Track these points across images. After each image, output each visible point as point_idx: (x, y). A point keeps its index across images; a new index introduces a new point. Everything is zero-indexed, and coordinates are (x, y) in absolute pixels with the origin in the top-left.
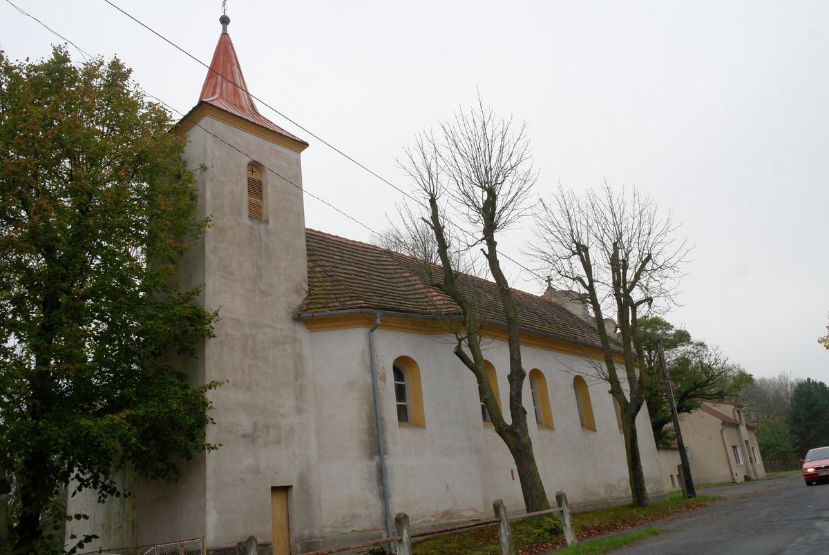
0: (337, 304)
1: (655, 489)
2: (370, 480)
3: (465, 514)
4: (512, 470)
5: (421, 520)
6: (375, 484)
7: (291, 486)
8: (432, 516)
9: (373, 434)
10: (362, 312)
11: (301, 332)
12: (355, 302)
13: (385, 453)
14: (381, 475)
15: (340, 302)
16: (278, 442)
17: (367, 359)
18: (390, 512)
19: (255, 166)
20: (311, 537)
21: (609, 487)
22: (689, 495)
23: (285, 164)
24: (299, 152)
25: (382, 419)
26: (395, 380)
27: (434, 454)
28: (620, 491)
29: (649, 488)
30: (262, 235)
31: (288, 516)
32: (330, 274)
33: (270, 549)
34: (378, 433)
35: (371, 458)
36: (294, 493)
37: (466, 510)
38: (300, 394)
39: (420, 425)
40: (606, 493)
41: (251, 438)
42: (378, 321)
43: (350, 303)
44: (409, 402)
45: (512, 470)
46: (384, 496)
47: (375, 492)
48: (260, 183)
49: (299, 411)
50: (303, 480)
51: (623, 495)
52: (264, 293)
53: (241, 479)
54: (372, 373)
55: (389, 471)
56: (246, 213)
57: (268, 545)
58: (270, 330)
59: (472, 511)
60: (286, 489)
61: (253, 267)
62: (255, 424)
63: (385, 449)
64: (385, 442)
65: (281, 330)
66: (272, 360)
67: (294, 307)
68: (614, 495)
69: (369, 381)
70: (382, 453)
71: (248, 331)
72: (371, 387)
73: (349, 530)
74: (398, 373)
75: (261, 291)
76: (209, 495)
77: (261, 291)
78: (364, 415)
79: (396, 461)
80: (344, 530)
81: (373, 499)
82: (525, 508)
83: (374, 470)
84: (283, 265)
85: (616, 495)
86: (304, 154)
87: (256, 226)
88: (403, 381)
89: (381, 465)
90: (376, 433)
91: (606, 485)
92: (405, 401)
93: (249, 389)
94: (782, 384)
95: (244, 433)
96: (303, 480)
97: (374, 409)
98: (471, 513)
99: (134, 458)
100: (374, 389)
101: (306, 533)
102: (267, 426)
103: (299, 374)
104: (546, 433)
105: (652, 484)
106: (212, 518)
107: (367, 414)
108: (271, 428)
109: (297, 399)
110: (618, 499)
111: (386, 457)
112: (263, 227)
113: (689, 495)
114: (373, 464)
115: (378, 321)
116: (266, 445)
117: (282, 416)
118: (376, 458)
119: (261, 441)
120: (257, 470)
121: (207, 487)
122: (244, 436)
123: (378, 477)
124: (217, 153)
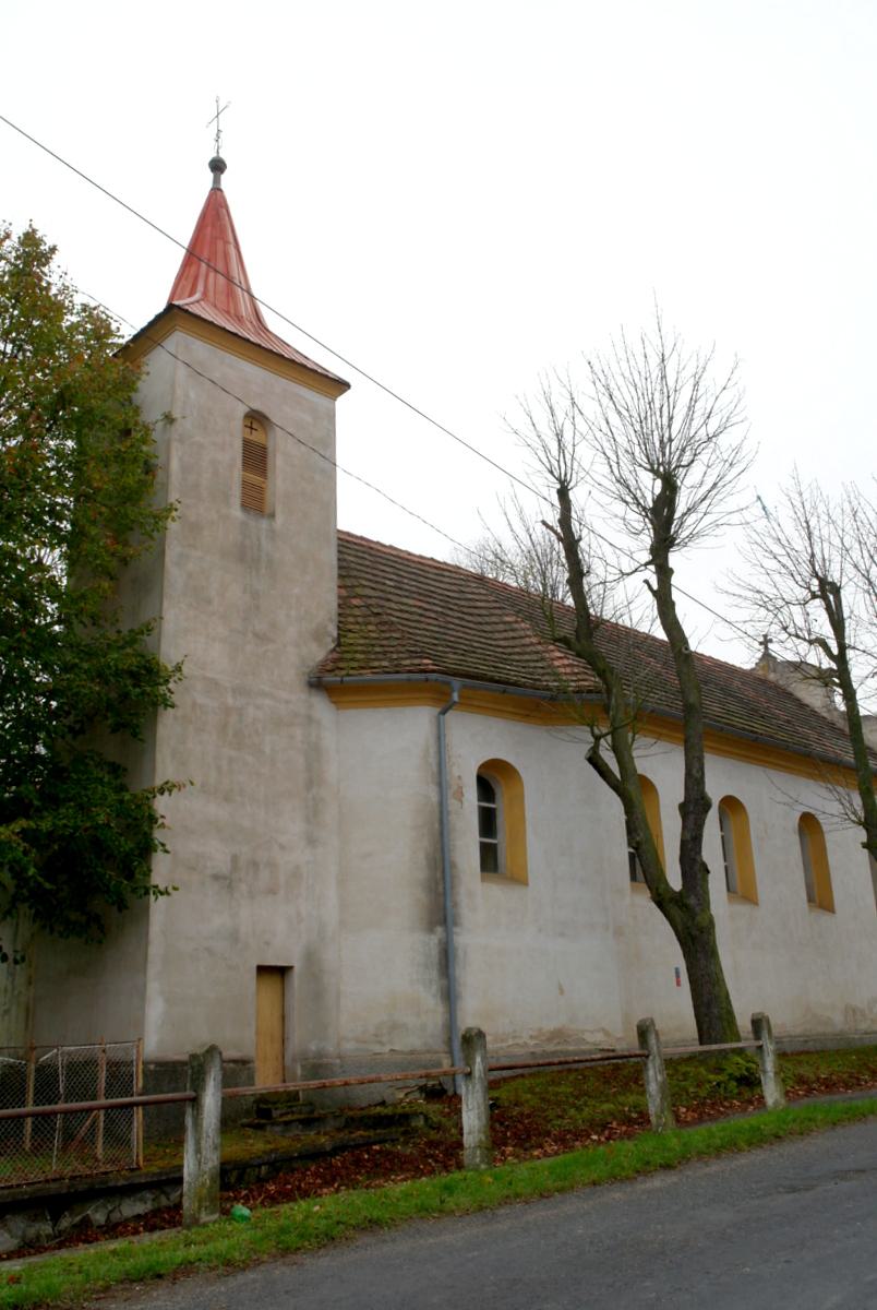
0: (385, 663)
3: (589, 1038)
6: (434, 974)
8: (531, 1037)
11: (321, 706)
12: (416, 661)
13: (455, 924)
14: (446, 961)
16: (272, 891)
17: (433, 760)
19: (256, 419)
20: (320, 1055)
23: (308, 418)
25: (453, 865)
26: (479, 800)
27: (540, 930)
31: (283, 1017)
35: (430, 929)
36: (296, 979)
37: (592, 1032)
38: (313, 814)
39: (519, 879)
43: (407, 662)
44: (502, 840)
46: (449, 996)
50: (311, 958)
52: (262, 638)
55: (460, 953)
56: (236, 500)
58: (268, 702)
60: (282, 972)
61: (244, 592)
62: (234, 859)
64: (455, 905)
65: (287, 702)
67: (312, 664)
69: (435, 798)
71: (230, 701)
72: (437, 810)
73: (387, 1049)
74: (486, 788)
75: (256, 635)
76: (153, 969)
77: (256, 635)
78: (421, 856)
79: (472, 939)
80: (377, 1048)
83: (435, 952)
84: (296, 591)
85: (863, 1026)
88: (493, 802)
93: (227, 799)
98: (599, 1037)
100: (441, 812)
101: (313, 1047)
102: (255, 864)
104: (744, 909)
106: (155, 1011)
110: (866, 1033)
112: (264, 524)
114: (434, 940)
115: (455, 696)
117: (282, 847)
118: (439, 930)
119: (244, 887)
120: (234, 937)
122: (216, 877)
123: (440, 964)
124: (192, 395)
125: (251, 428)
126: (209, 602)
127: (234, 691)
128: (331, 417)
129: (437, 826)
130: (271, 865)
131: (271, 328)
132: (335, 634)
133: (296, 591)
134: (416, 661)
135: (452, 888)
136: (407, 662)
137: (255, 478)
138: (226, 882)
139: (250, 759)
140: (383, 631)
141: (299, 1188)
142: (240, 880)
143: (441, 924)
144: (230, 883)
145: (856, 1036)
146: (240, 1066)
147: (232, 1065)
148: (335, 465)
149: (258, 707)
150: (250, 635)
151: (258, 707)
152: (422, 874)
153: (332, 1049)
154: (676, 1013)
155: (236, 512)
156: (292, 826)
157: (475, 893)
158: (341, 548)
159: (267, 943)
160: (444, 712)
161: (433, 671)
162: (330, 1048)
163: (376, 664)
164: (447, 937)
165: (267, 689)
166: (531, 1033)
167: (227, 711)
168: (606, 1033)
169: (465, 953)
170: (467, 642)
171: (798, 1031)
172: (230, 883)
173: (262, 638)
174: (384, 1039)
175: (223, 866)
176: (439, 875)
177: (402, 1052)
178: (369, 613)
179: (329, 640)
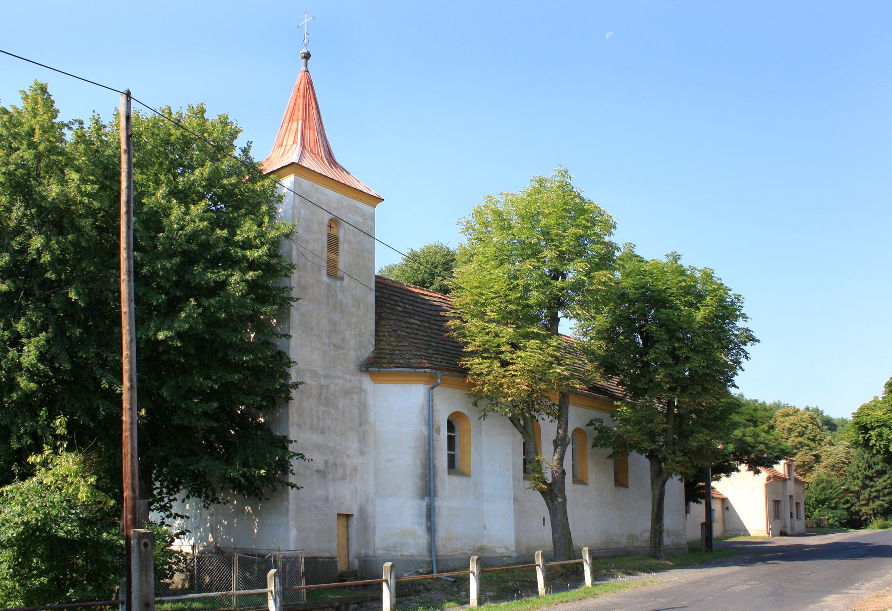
0: (401, 361)
1: (676, 541)
2: (419, 516)
3: (498, 551)
4: (544, 518)
5: (459, 552)
6: (424, 520)
7: (353, 515)
8: (469, 550)
9: (426, 479)
10: (425, 372)
11: (367, 382)
12: (419, 361)
13: (435, 496)
14: (430, 514)
15: (405, 359)
16: (344, 478)
17: (426, 413)
18: (436, 418)
19: (334, 222)
20: (367, 556)
21: (632, 537)
22: (706, 549)
23: (360, 220)
24: (374, 206)
25: (434, 466)
26: (448, 432)
27: (476, 498)
28: (642, 542)
29: (667, 541)
30: (338, 291)
31: (348, 539)
32: (394, 329)
33: (335, 561)
34: (430, 478)
35: (422, 498)
36: (354, 521)
37: (499, 548)
38: (363, 439)
39: (465, 474)
40: (628, 542)
41: (323, 474)
42: (439, 381)
43: (414, 361)
44: (457, 452)
45: (544, 518)
46: (431, 530)
47: (424, 526)
48: (337, 238)
49: (362, 453)
50: (362, 510)
51: (644, 545)
52: (337, 347)
53: (314, 506)
54: (429, 426)
55: (437, 510)
56: (324, 271)
57: (335, 558)
58: (341, 381)
59: (504, 549)
60: (348, 516)
61: (329, 322)
62: (326, 462)
63: (435, 492)
64: (435, 486)
65: (350, 381)
66: (341, 407)
67: (362, 360)
68: (634, 545)
69: (426, 433)
70: (432, 495)
71: (323, 382)
72: (427, 439)
73: (399, 554)
74: (451, 426)
75: (335, 346)
76: (291, 515)
77: (335, 346)
78: (418, 462)
79: (445, 503)
80: (395, 554)
81: (421, 531)
82: (553, 550)
83: (424, 509)
84: (354, 320)
85: (636, 544)
86: (380, 205)
87: (333, 283)
88: (454, 432)
89: (430, 505)
90: (428, 479)
91: (629, 535)
92: (454, 451)
93: (322, 432)
94: (588, 479)
95: (317, 469)
96: (362, 510)
97: (428, 457)
98: (503, 550)
99: (861, 513)
100: (429, 440)
101: (363, 552)
102: (335, 465)
103: (363, 421)
104: (579, 487)
105: (674, 537)
106: (293, 534)
107: (422, 462)
108: (339, 466)
109: (360, 442)
110: (638, 548)
111: (435, 499)
112: (338, 283)
113: (706, 549)
114: (424, 504)
115: (439, 381)
116: (334, 480)
117: (348, 456)
118: (427, 498)
119: (330, 476)
120: (327, 500)
121: (290, 510)
122: (318, 471)
123: (427, 515)
124: (302, 212)
125: (330, 227)
126: (312, 329)
127: (324, 376)
128: (373, 218)
129: (427, 447)
130: (343, 465)
131: (337, 161)
132: (374, 343)
133: (354, 320)
134: (419, 361)
135: (434, 478)
136: (414, 361)
137: (333, 256)
138: (322, 474)
139: (332, 411)
140: (399, 342)
141: (613, 331)
142: (329, 472)
143: (428, 496)
144: (324, 474)
145: (633, 549)
146: (331, 560)
147: (328, 560)
148: (370, 235)
149: (336, 384)
150: (332, 345)
151: (336, 384)
152: (419, 471)
153: (371, 553)
154: (545, 535)
155: (325, 278)
156: (353, 445)
157: (446, 482)
158: (379, 285)
159: (342, 503)
160: (432, 388)
161: (428, 368)
162: (371, 553)
163: (397, 361)
164: (431, 502)
165: (340, 374)
166: (469, 548)
167: (322, 386)
168: (507, 548)
169: (439, 509)
170: (442, 346)
171: (603, 547)
172: (324, 474)
173: (337, 347)
174: (398, 549)
175: (322, 467)
176: (427, 472)
177: (407, 556)
178: (390, 330)
179: (371, 346)
